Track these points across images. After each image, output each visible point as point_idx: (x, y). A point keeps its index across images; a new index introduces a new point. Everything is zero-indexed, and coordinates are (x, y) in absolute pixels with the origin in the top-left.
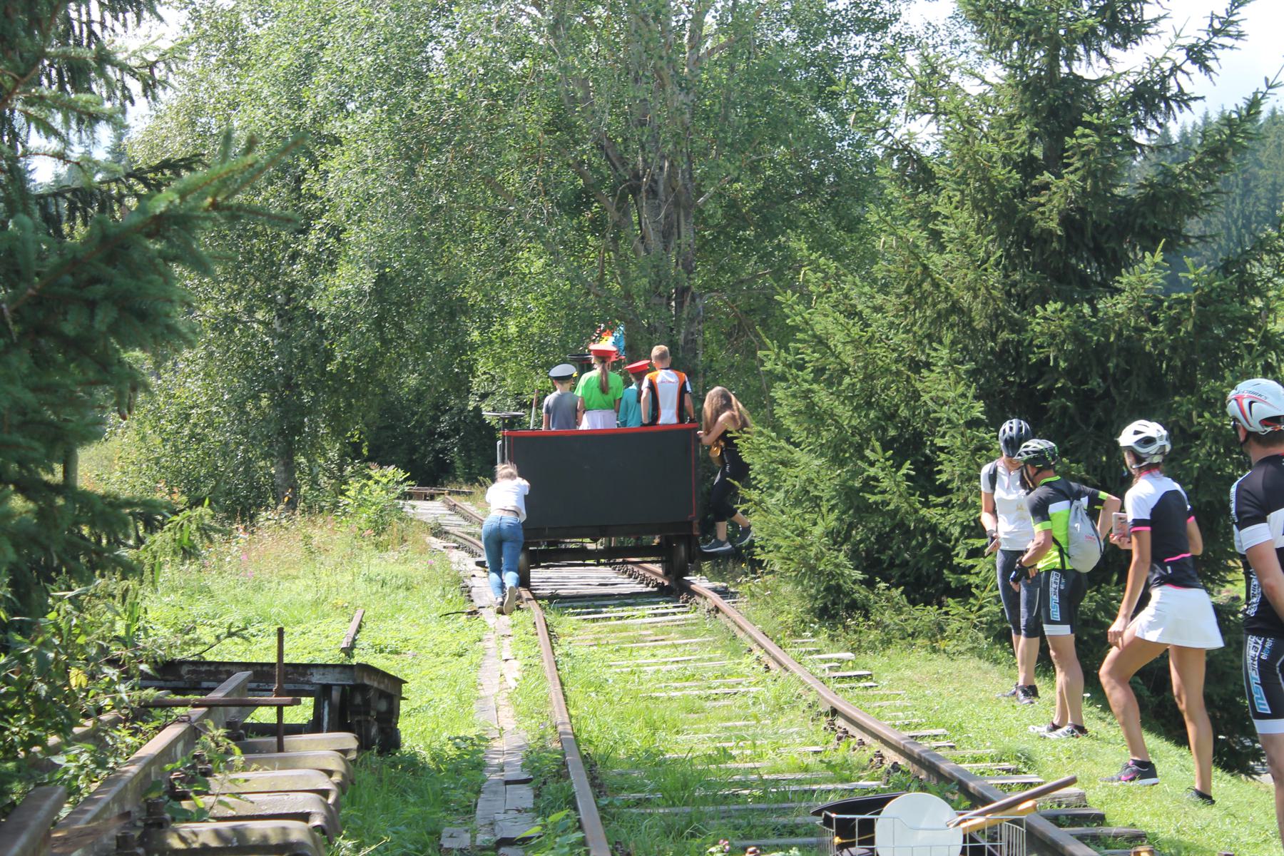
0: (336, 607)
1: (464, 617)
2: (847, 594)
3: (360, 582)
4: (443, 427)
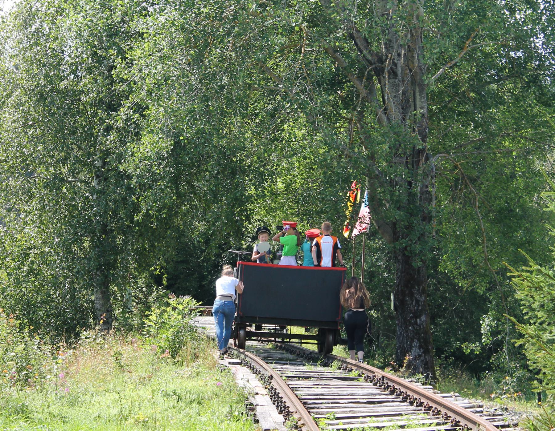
0: (137, 422)
3: (159, 398)
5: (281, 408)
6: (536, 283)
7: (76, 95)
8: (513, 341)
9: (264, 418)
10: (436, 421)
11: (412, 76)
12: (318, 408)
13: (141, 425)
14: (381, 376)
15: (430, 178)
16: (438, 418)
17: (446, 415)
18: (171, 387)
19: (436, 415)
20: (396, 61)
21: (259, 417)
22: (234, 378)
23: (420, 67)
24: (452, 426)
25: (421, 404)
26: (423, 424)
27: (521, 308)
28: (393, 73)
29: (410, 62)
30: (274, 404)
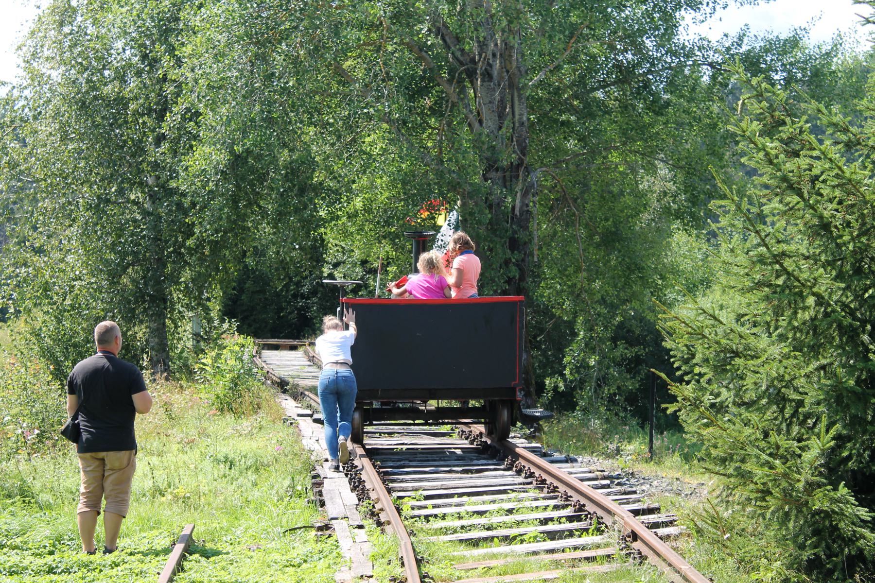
0: (176, 498)
1: (313, 532)
2: (851, 541)
3: (207, 464)
4: (305, 289)
5: (355, 483)
6: (698, 328)
7: (121, 102)
8: (663, 406)
9: (332, 498)
10: (553, 503)
11: (510, 77)
12: (402, 481)
13: (181, 501)
14: (478, 433)
15: (531, 196)
16: (555, 498)
17: (566, 494)
18: (223, 450)
19: (552, 492)
20: (491, 61)
21: (326, 497)
22: (299, 434)
23: (518, 68)
24: (575, 511)
25: (532, 475)
26: (537, 507)
27: (672, 360)
28: (488, 75)
29: (507, 62)
30: (346, 475)
